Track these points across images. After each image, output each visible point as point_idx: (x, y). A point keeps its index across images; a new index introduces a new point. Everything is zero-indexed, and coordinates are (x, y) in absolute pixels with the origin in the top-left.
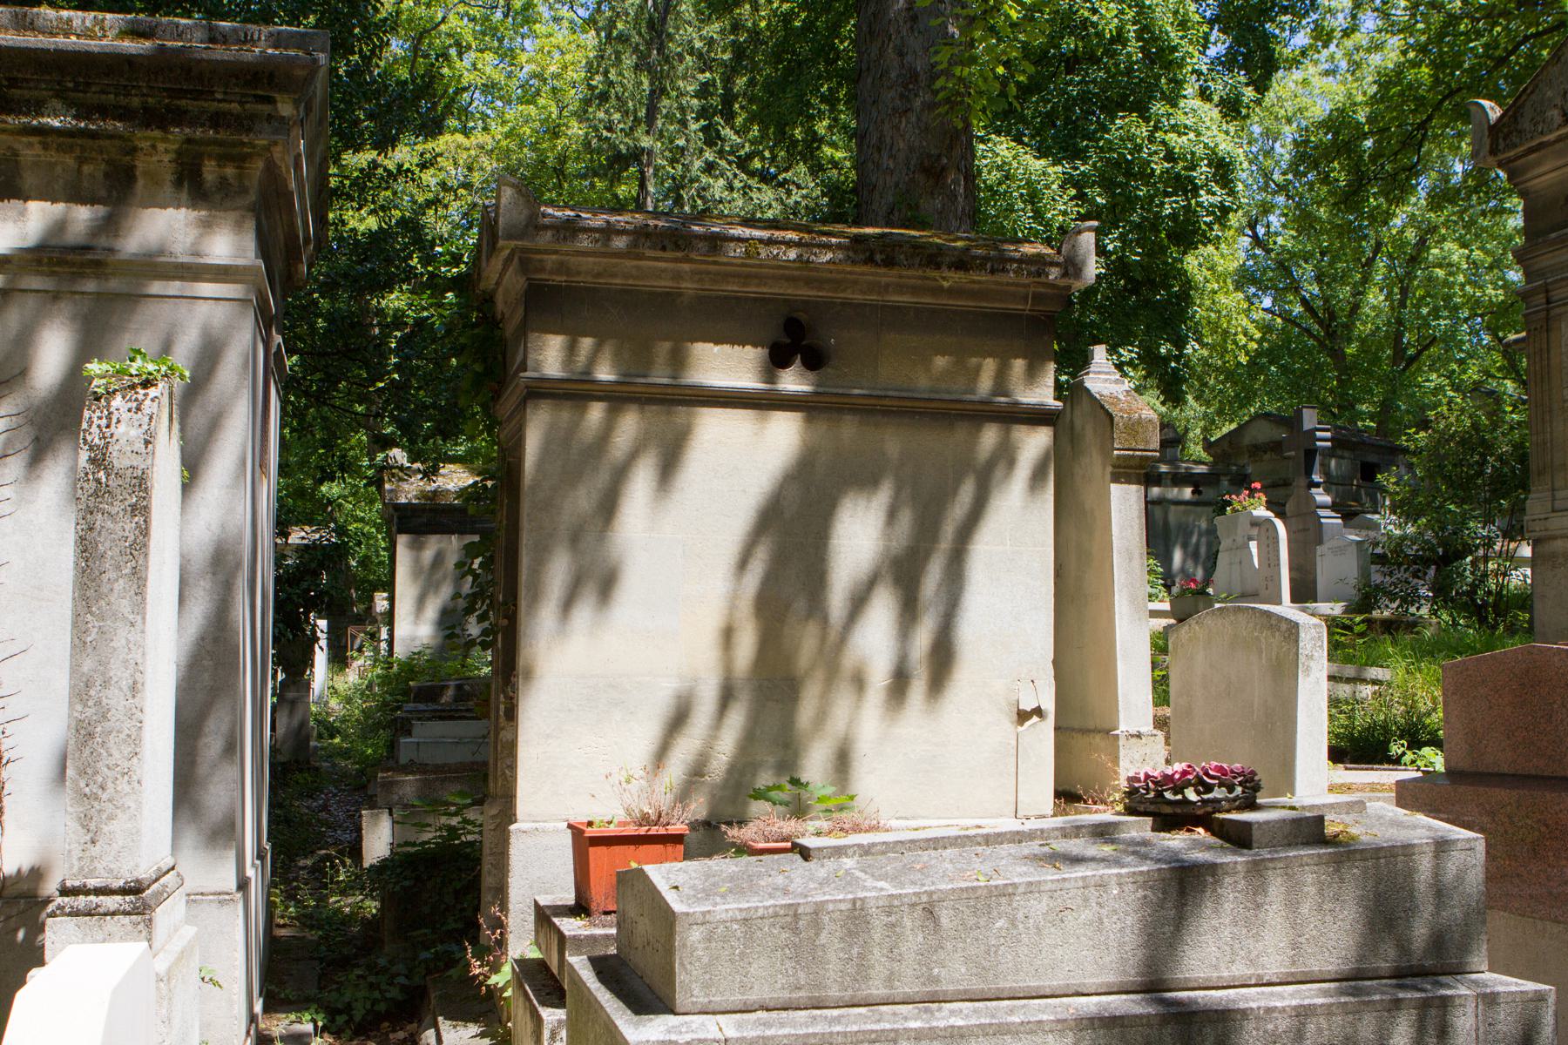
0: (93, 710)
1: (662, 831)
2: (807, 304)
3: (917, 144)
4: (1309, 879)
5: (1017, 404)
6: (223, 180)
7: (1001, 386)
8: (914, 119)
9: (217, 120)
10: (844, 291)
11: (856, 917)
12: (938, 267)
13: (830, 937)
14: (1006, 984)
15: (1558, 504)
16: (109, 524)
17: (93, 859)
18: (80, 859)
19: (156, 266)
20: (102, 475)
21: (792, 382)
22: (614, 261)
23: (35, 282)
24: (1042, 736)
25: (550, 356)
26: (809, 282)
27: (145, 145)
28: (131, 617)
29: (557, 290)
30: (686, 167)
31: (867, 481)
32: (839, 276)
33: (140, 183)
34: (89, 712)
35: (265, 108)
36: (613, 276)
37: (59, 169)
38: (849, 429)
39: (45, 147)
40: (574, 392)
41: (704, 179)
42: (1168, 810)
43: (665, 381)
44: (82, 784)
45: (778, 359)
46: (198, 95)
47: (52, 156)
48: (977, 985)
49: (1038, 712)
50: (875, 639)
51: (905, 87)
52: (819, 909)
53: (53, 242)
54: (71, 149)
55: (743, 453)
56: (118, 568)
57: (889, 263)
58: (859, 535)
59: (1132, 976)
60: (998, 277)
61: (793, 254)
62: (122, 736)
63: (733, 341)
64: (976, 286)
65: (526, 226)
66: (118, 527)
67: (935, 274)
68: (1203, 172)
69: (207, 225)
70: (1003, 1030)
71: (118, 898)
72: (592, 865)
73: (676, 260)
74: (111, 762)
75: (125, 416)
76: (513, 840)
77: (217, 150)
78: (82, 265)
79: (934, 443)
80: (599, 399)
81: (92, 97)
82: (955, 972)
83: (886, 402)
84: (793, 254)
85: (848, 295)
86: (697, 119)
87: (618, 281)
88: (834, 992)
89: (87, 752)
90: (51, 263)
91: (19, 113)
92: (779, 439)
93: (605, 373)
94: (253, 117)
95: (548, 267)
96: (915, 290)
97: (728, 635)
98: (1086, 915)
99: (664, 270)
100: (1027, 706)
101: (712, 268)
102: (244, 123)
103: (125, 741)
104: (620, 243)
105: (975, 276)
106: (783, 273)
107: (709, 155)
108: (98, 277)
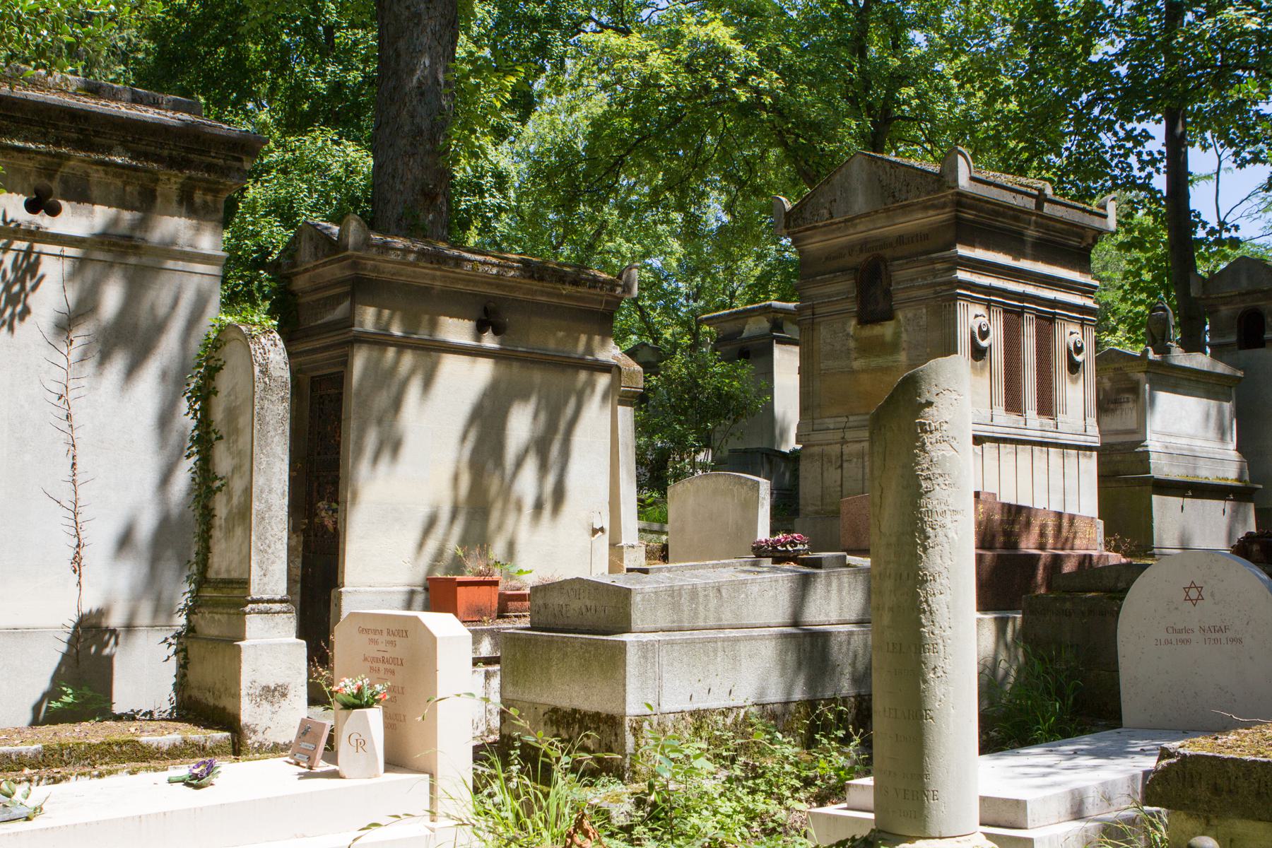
4: (845, 579)
6: (205, 203)
7: (589, 349)
9: (210, 168)
11: (694, 592)
12: (564, 283)
13: (685, 600)
14: (745, 622)
15: (816, 427)
19: (168, 250)
21: (489, 342)
23: (99, 255)
24: (603, 541)
25: (368, 318)
26: (498, 286)
27: (164, 177)
31: (524, 396)
33: (159, 200)
35: (237, 164)
37: (112, 187)
38: (516, 368)
39: (106, 173)
40: (380, 340)
42: (778, 555)
43: (426, 337)
45: (480, 329)
46: (202, 153)
47: (110, 179)
48: (734, 622)
49: (602, 530)
50: (527, 483)
52: (681, 588)
53: (111, 231)
54: (120, 176)
55: (464, 379)
57: (541, 279)
58: (521, 425)
59: (788, 620)
60: (592, 291)
61: (495, 271)
63: (459, 317)
67: (559, 286)
68: (488, 181)
69: (198, 230)
70: (752, 638)
77: (204, 185)
78: (127, 247)
79: (557, 379)
80: (392, 345)
81: (141, 147)
82: (727, 618)
85: (516, 295)
88: (686, 624)
90: (110, 244)
91: (98, 152)
92: (483, 371)
93: (396, 331)
94: (229, 168)
96: (549, 294)
97: (456, 478)
98: (771, 593)
102: (225, 172)
104: (411, 257)
105: (582, 290)
106: (487, 280)
108: (135, 254)
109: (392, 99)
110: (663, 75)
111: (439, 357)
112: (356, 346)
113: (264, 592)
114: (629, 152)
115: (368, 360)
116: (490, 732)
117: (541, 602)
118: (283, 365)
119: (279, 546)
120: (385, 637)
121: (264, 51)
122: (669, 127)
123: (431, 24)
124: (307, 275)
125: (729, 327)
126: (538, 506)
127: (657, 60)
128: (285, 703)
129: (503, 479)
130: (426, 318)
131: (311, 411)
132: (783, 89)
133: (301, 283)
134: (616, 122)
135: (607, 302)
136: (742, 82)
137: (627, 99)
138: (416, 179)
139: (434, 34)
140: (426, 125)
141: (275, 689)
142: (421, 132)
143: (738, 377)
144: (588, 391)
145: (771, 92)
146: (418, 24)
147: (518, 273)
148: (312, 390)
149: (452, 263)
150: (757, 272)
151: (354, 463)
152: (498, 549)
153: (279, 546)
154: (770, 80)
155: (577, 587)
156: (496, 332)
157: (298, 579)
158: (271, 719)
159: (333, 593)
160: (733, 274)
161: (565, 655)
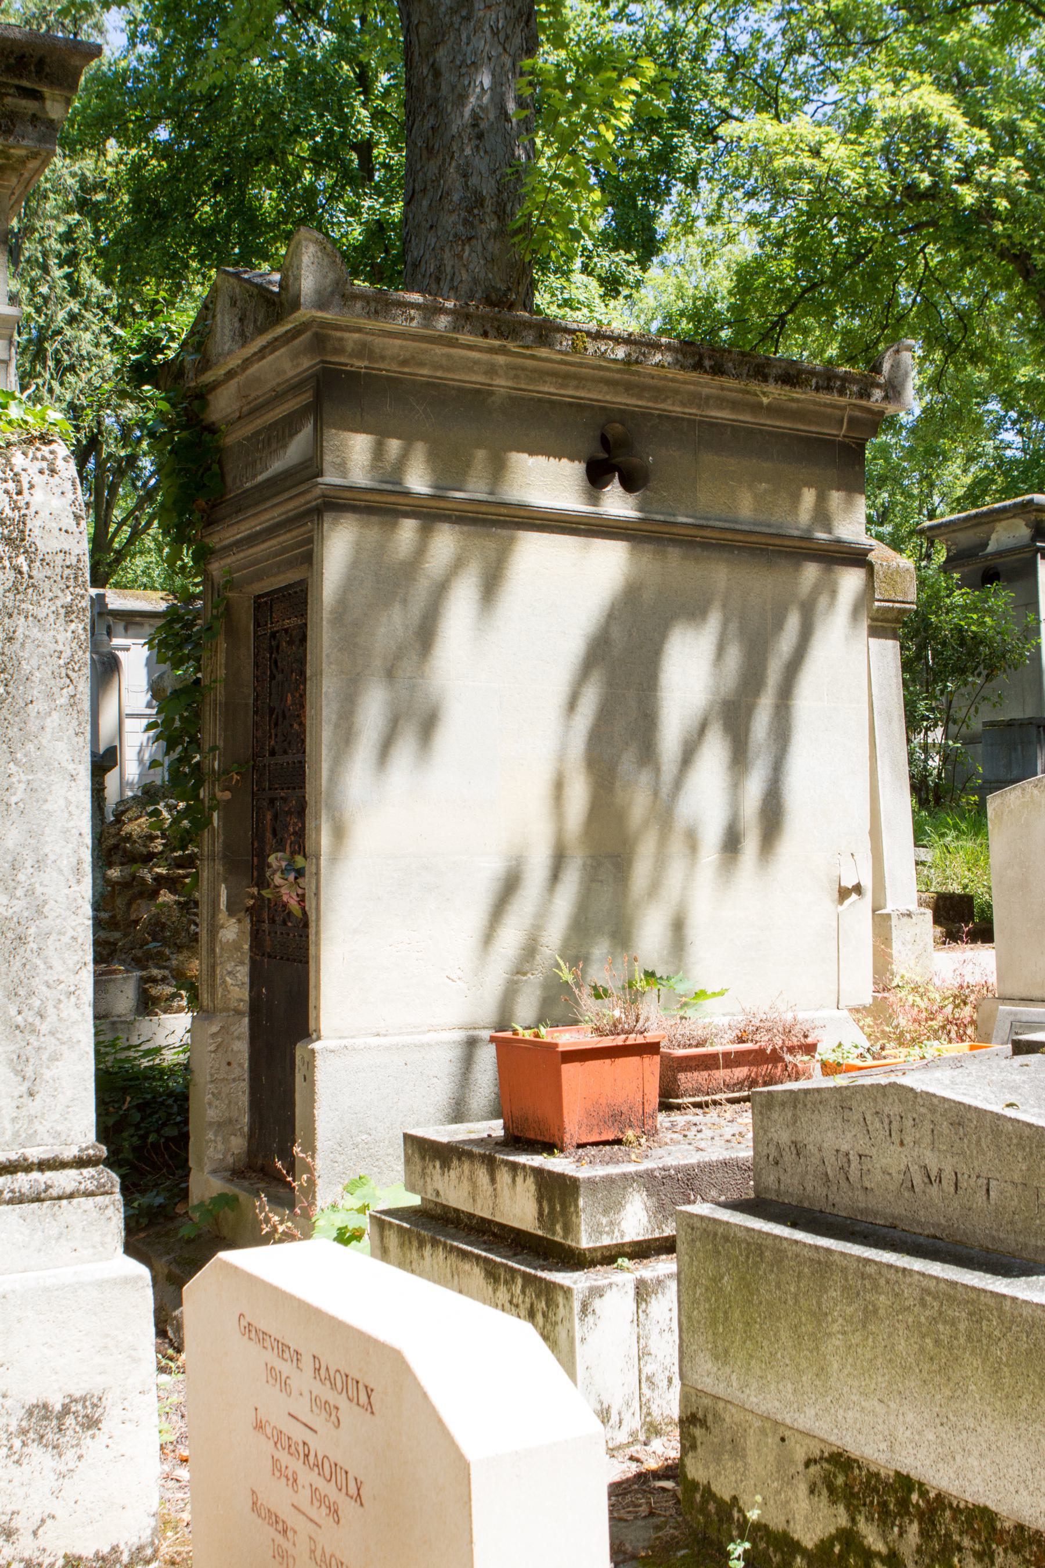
0: (23, 903)
1: (640, 1040)
2: (623, 415)
3: (482, 275)
5: (839, 541)
7: (823, 517)
8: (479, 248)
10: (664, 401)
12: (765, 379)
16: (35, 633)
17: (31, 1119)
18: (14, 1120)
20: (21, 560)
21: (617, 504)
22: (424, 346)
24: (860, 909)
25: (355, 456)
26: (629, 388)
28: (71, 767)
29: (354, 376)
30: (50, 319)
32: (661, 383)
34: (19, 905)
35: (29, 106)
36: (422, 364)
40: (382, 505)
41: (69, 333)
44: (13, 1012)
45: (596, 476)
49: (858, 889)
50: (707, 794)
51: (470, 211)
56: (50, 696)
57: (718, 370)
58: (690, 671)
60: (824, 397)
61: (621, 352)
62: (66, 939)
63: (549, 453)
64: (794, 405)
65: (332, 293)
66: (48, 638)
67: (754, 386)
71: (72, 1173)
72: (565, 1087)
73: (492, 350)
74: (51, 977)
75: (38, 479)
76: (319, 1062)
79: (761, 583)
80: (407, 515)
83: (707, 533)
84: (621, 352)
86: (61, 266)
87: (425, 372)
89: (17, 964)
92: (602, 569)
93: (418, 482)
95: (349, 349)
96: (735, 405)
97: (559, 787)
99: (477, 362)
100: (849, 884)
101: (529, 363)
103: (69, 946)
105: (798, 394)
107: (74, 306)
109: (430, 150)
110: (848, 172)
111: (512, 540)
112: (328, 518)
113: (31, 1140)
114: (791, 310)
115: (358, 548)
116: (653, 1430)
117: (784, 1137)
118: (69, 523)
119: (68, 1010)
120: (303, 1380)
121: (280, 198)
122: (849, 267)
123: (491, 14)
124: (233, 383)
125: (965, 538)
126: (732, 843)
127: (836, 152)
128: (93, 1445)
129: (656, 793)
130: (481, 454)
131: (257, 665)
132: (1027, 184)
133: (223, 405)
134: (772, 266)
135: (852, 420)
136: (965, 179)
137: (786, 235)
138: (475, 281)
139: (495, 33)
140: (488, 189)
141: (66, 1410)
142: (480, 201)
143: (991, 612)
144: (823, 600)
145: (1007, 191)
146: (467, 19)
147: (669, 358)
148: (257, 624)
149: (530, 336)
150: (968, 480)
151: (333, 772)
152: (651, 936)
153: (68, 1010)
154: (1010, 171)
155: (893, 1109)
156: (629, 485)
157: (244, 1007)
158: (56, 1494)
159: (299, 1051)
160: (932, 485)
161: (870, 1313)
